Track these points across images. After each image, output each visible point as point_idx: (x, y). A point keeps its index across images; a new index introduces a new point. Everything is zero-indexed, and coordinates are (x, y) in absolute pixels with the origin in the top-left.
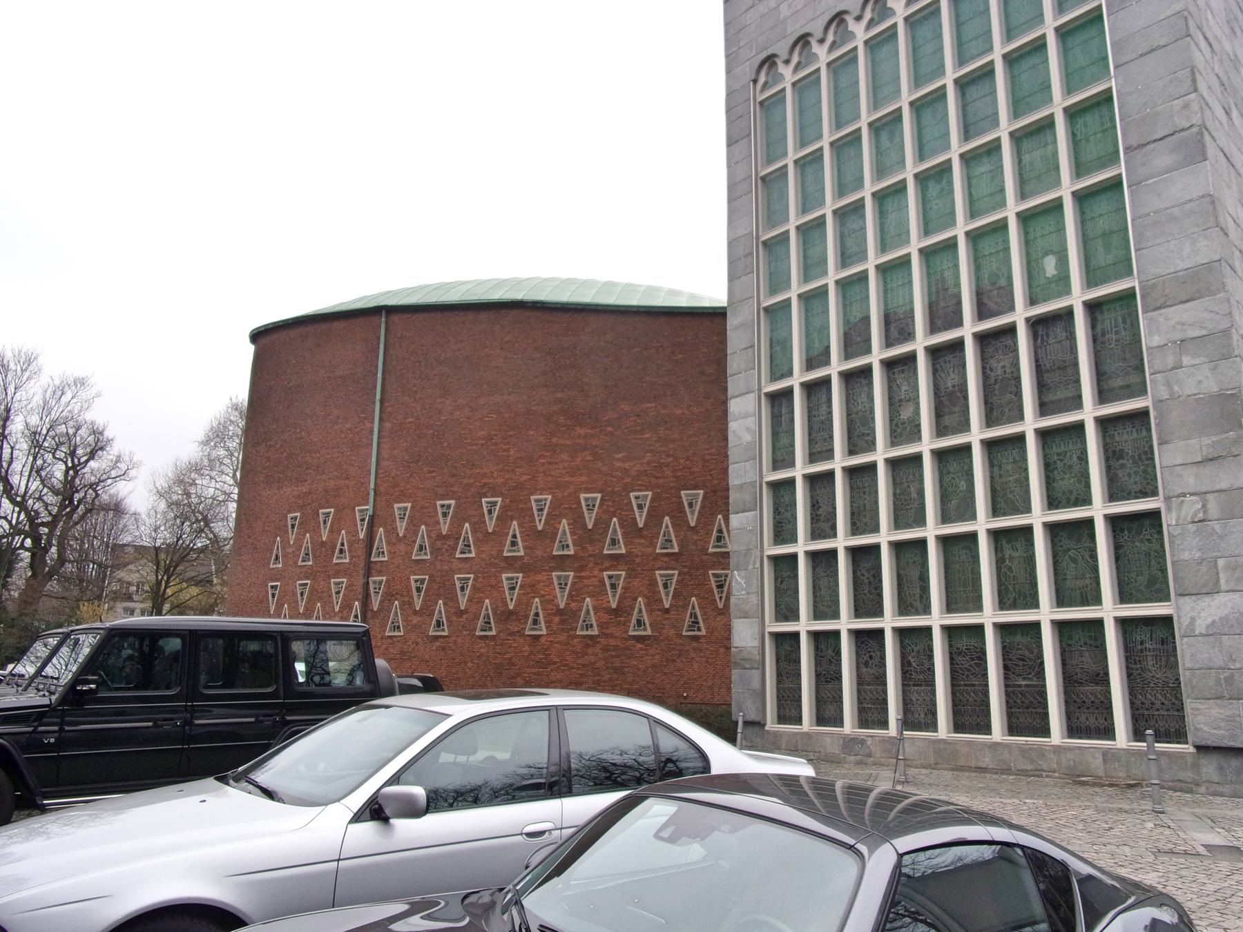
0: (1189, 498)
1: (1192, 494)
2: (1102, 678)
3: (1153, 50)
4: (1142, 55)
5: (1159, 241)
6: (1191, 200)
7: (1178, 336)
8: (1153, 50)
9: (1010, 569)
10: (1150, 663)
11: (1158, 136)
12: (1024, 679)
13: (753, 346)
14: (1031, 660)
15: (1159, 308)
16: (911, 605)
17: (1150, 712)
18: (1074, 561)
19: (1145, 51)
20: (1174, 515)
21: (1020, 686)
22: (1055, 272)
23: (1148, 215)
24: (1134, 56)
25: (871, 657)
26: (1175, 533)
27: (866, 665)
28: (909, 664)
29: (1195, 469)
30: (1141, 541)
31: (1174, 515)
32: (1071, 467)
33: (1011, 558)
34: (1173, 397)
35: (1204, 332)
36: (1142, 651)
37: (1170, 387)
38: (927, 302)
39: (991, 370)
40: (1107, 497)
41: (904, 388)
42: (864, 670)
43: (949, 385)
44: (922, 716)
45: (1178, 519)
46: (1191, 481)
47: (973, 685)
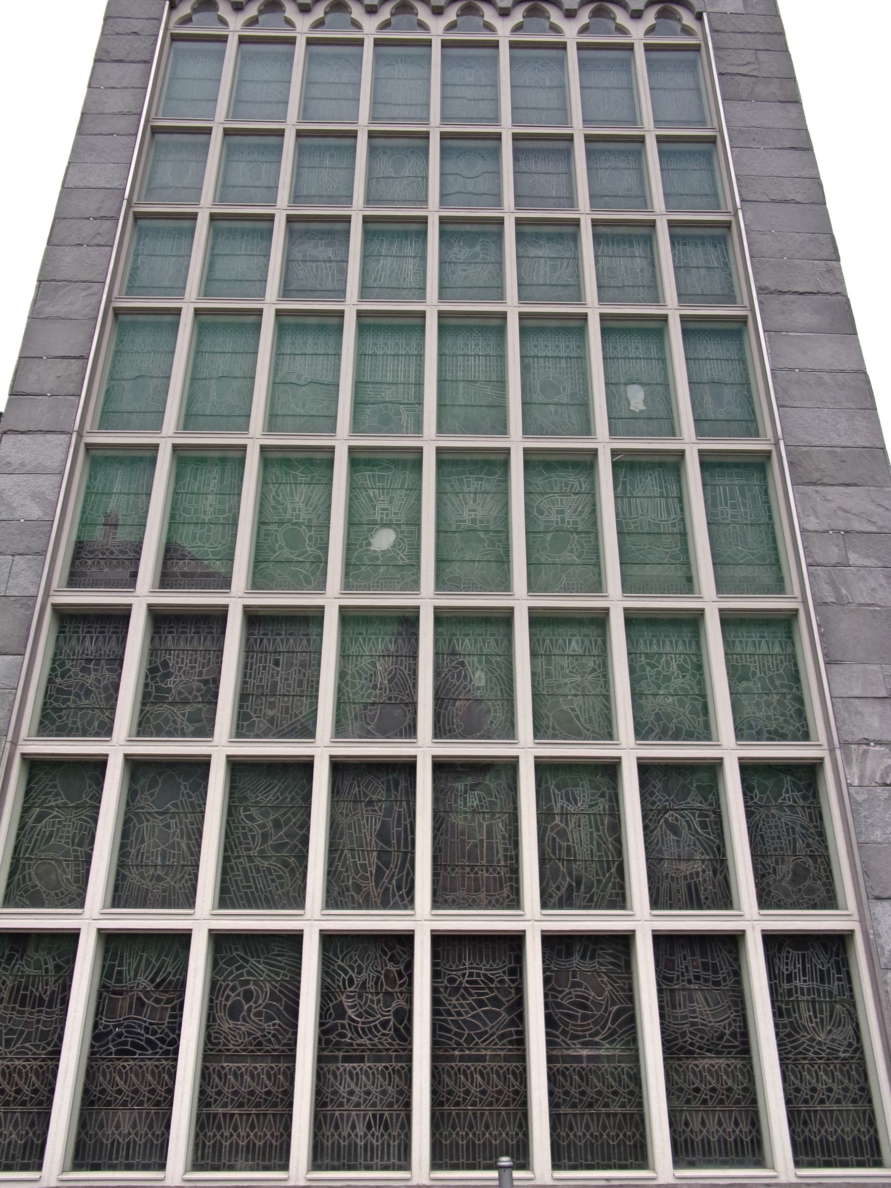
0: (874, 749)
1: (878, 743)
2: (742, 1045)
3: (786, 202)
4: (773, 201)
5: (807, 404)
6: (842, 371)
7: (841, 525)
8: (786, 202)
9: (562, 834)
10: (806, 1014)
11: (801, 291)
12: (585, 1045)
13: (84, 358)
14: (598, 1005)
15: (815, 484)
16: (358, 888)
17: (827, 1106)
18: (675, 830)
19: (778, 198)
20: (855, 770)
21: (579, 1059)
22: (642, 407)
23: (791, 370)
24: (765, 198)
25: (248, 996)
26: (860, 798)
27: (234, 1012)
28: (341, 1012)
29: (878, 707)
30: (780, 807)
31: (855, 770)
32: (667, 679)
33: (564, 814)
34: (840, 602)
35: (873, 529)
36: (790, 992)
37: (836, 590)
38: (164, 541)
39: (541, 513)
40: (109, 900)
41: (379, 505)
42: (227, 1025)
43: (466, 515)
44: (361, 1130)
45: (861, 777)
46: (875, 722)
47: (482, 1058)
